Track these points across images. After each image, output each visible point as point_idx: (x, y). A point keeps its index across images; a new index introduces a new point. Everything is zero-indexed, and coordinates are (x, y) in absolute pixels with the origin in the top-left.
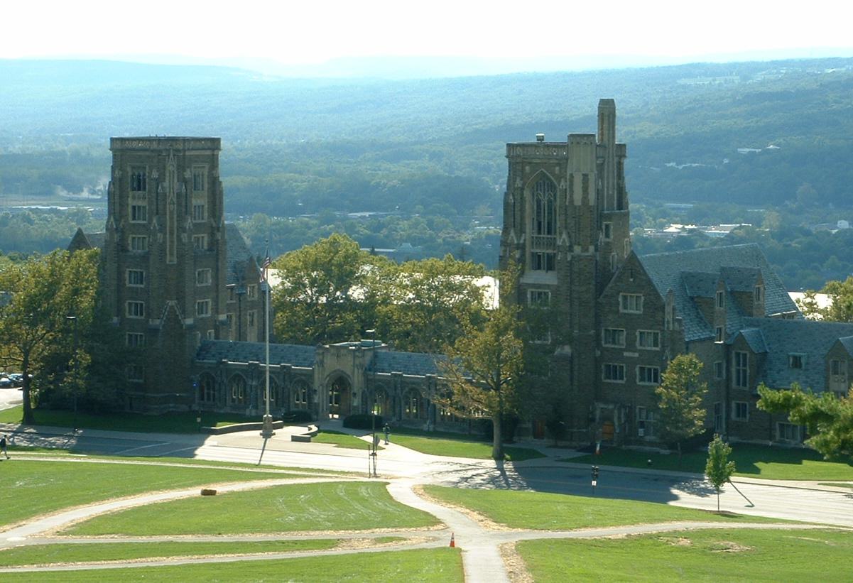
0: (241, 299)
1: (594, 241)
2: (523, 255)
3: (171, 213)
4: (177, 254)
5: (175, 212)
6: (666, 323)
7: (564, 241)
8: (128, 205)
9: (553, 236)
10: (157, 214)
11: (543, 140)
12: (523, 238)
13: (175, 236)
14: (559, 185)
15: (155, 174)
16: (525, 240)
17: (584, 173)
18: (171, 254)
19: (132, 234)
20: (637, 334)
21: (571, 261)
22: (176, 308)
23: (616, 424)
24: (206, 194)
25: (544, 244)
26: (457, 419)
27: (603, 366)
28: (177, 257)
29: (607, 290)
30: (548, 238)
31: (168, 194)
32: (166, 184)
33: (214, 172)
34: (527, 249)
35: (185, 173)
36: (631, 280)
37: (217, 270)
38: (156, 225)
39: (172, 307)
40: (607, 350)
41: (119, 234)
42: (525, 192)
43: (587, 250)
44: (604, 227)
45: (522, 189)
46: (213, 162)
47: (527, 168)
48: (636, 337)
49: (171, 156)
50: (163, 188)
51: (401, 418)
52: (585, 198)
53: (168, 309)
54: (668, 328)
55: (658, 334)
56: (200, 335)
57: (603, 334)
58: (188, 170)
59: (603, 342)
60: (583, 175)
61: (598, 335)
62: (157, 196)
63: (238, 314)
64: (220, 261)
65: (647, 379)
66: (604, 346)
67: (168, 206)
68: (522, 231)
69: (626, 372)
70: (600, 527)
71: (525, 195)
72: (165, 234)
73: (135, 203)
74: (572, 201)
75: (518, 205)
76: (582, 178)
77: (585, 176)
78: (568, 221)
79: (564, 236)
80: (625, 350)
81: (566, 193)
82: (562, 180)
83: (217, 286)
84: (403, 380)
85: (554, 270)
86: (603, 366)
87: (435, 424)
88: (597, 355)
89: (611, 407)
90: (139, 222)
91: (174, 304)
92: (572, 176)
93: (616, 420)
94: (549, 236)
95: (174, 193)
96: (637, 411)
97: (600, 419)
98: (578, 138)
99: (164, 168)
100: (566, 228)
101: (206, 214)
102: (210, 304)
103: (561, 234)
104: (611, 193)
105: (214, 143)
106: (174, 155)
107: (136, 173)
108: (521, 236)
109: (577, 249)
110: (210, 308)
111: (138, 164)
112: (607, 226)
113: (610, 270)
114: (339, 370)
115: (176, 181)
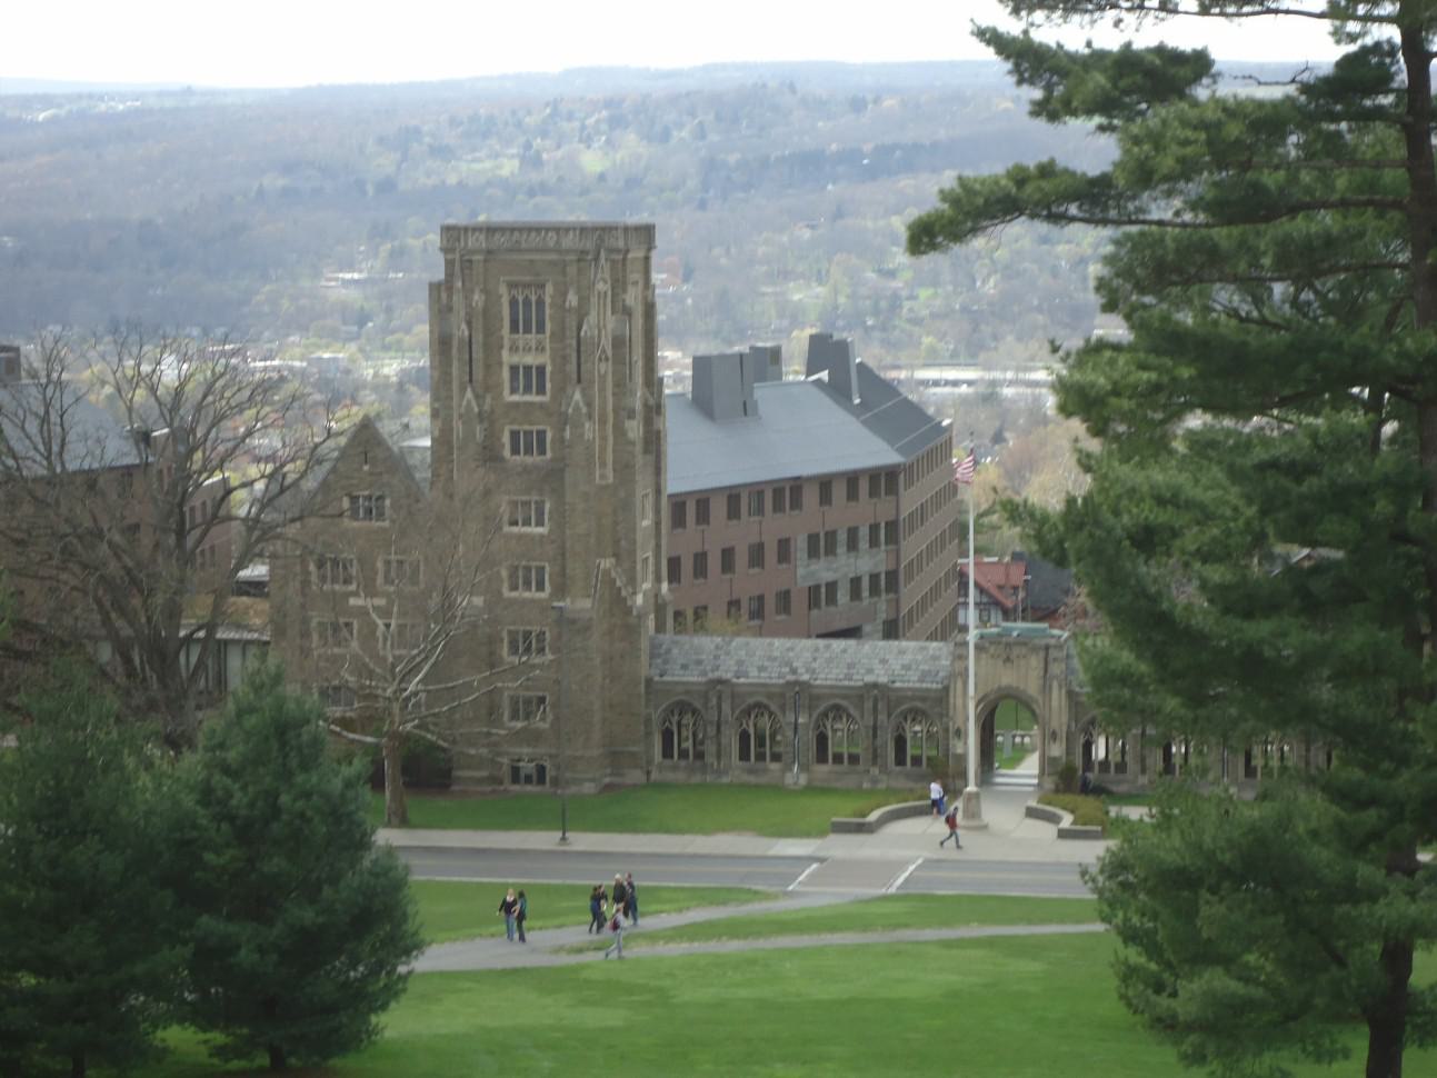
4: (614, 463)
8: (500, 364)
10: (579, 381)
19: (511, 423)
28: (614, 470)
38: (581, 404)
39: (607, 572)
41: (486, 425)
73: (515, 359)
75: (479, 338)
106: (606, 260)
111: (527, 278)
115: (609, 312)
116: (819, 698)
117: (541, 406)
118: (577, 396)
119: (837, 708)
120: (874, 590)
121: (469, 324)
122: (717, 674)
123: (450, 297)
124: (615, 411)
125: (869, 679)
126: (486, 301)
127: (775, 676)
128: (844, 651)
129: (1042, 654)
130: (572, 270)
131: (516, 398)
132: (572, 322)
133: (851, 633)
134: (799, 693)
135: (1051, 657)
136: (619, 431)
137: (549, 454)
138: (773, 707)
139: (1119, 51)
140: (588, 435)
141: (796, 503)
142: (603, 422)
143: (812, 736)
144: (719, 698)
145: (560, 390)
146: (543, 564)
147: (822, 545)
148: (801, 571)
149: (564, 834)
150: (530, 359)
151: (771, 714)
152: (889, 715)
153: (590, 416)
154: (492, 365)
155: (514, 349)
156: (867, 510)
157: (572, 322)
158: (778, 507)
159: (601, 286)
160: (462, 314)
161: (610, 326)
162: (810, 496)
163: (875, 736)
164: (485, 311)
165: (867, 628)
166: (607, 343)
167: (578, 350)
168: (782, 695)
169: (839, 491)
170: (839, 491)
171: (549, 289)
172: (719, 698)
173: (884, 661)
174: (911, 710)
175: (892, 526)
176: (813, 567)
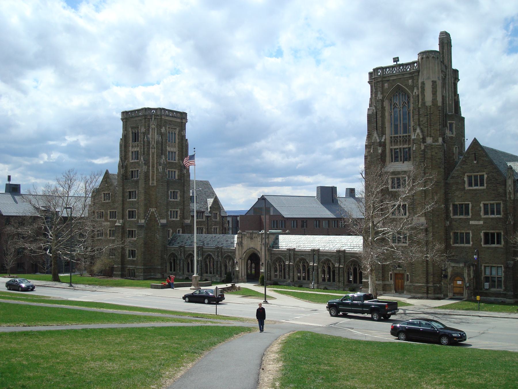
0: (209, 219)
1: (443, 135)
2: (384, 151)
3: (153, 154)
4: (156, 179)
5: (155, 153)
6: (507, 194)
7: (418, 134)
10: (144, 154)
11: (398, 61)
12: (384, 138)
13: (155, 168)
14: (413, 93)
15: (143, 130)
16: (385, 140)
17: (433, 80)
18: (153, 180)
20: (482, 205)
21: (424, 150)
22: (155, 213)
23: (467, 279)
24: (177, 145)
25: (400, 141)
27: (451, 234)
29: (455, 173)
30: (403, 136)
31: (151, 142)
32: (150, 136)
33: (182, 133)
34: (387, 146)
35: (161, 129)
36: (475, 162)
37: (184, 192)
38: (143, 161)
39: (153, 213)
40: (456, 220)
41: (124, 169)
42: (384, 103)
43: (437, 141)
44: (448, 125)
45: (382, 101)
46: (182, 126)
47: (386, 85)
48: (480, 208)
49: (153, 118)
50: (147, 138)
51: (294, 280)
52: (434, 100)
53: (150, 213)
54: (510, 198)
55: (500, 204)
56: (171, 231)
57: (451, 209)
58: (164, 128)
59: (451, 215)
60: (432, 81)
61: (447, 208)
62: (144, 143)
63: (207, 227)
64: (185, 187)
65: (490, 241)
66: (452, 217)
67: (151, 149)
68: (383, 133)
69: (472, 237)
71: (384, 106)
72: (149, 167)
73: (133, 150)
74: (424, 103)
76: (431, 84)
77: (434, 82)
78: (421, 119)
79: (418, 131)
80: (471, 219)
81: (418, 98)
82: (415, 88)
83: (184, 201)
84: (295, 253)
85: (409, 160)
86: (451, 234)
87: (318, 283)
88: (447, 225)
89: (461, 265)
91: (154, 210)
92: (423, 83)
93: (466, 275)
94: (405, 135)
95: (154, 141)
96: (483, 268)
97: (452, 276)
98: (427, 53)
99: (149, 127)
100: (419, 125)
101: (177, 158)
102: (179, 213)
103: (415, 130)
104: (450, 103)
105: (183, 116)
107: (134, 132)
108: (382, 136)
109: (429, 140)
110: (179, 215)
112: (451, 125)
113: (454, 159)
114: (252, 248)
115: (156, 134)
116: (205, 252)
124: (157, 163)
129: (261, 236)
131: (133, 161)
139: (462, 117)
146: (485, 246)
149: (265, 300)
152: (222, 258)
164: (147, 141)
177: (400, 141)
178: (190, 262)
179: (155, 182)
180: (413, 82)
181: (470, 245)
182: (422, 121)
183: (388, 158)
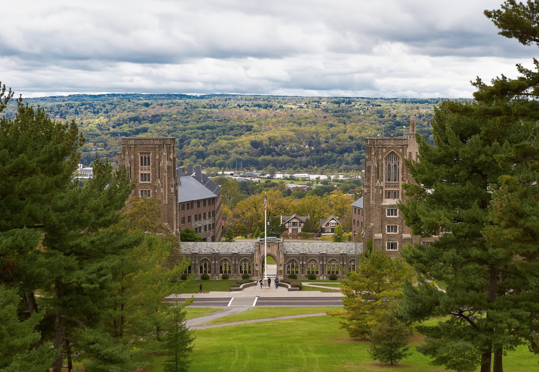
8: (138, 173)
9: (397, 182)
10: (159, 178)
19: (141, 188)
25: (392, 186)
26: (48, 299)
30: (394, 183)
47: (384, 150)
70: (429, 328)
73: (142, 172)
78: (408, 175)
90: (146, 182)
92: (410, 153)
117: (149, 184)
118: (159, 182)
119: (225, 259)
120: (210, 229)
121: (130, 163)
122: (194, 252)
123: (124, 156)
125: (233, 252)
126: (134, 158)
127: (209, 251)
128: (226, 245)
129: (277, 245)
130: (157, 150)
131: (141, 182)
132: (157, 162)
133: (205, 240)
134: (216, 256)
135: (279, 246)
136: (169, 190)
137: (151, 196)
138: (209, 260)
140: (162, 192)
141: (192, 207)
142: (165, 188)
143: (219, 266)
144: (195, 258)
145: (154, 180)
147: (198, 218)
148: (193, 224)
150: (146, 172)
151: (208, 261)
153: (162, 187)
154: (136, 174)
155: (142, 170)
156: (208, 209)
157: (157, 162)
158: (188, 208)
159: (164, 154)
160: (128, 161)
161: (167, 164)
162: (195, 205)
163: (235, 266)
165: (208, 238)
166: (166, 168)
167: (159, 170)
168: (211, 257)
169: (202, 204)
170: (202, 204)
171: (151, 154)
172: (195, 258)
173: (236, 247)
174: (244, 260)
175: (213, 212)
176: (196, 223)
177: (392, 186)
178: (203, 266)
179: (167, 201)
180: (403, 151)
181: (398, 216)
182: (409, 176)
183: (384, 196)
